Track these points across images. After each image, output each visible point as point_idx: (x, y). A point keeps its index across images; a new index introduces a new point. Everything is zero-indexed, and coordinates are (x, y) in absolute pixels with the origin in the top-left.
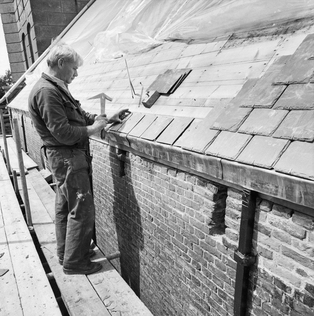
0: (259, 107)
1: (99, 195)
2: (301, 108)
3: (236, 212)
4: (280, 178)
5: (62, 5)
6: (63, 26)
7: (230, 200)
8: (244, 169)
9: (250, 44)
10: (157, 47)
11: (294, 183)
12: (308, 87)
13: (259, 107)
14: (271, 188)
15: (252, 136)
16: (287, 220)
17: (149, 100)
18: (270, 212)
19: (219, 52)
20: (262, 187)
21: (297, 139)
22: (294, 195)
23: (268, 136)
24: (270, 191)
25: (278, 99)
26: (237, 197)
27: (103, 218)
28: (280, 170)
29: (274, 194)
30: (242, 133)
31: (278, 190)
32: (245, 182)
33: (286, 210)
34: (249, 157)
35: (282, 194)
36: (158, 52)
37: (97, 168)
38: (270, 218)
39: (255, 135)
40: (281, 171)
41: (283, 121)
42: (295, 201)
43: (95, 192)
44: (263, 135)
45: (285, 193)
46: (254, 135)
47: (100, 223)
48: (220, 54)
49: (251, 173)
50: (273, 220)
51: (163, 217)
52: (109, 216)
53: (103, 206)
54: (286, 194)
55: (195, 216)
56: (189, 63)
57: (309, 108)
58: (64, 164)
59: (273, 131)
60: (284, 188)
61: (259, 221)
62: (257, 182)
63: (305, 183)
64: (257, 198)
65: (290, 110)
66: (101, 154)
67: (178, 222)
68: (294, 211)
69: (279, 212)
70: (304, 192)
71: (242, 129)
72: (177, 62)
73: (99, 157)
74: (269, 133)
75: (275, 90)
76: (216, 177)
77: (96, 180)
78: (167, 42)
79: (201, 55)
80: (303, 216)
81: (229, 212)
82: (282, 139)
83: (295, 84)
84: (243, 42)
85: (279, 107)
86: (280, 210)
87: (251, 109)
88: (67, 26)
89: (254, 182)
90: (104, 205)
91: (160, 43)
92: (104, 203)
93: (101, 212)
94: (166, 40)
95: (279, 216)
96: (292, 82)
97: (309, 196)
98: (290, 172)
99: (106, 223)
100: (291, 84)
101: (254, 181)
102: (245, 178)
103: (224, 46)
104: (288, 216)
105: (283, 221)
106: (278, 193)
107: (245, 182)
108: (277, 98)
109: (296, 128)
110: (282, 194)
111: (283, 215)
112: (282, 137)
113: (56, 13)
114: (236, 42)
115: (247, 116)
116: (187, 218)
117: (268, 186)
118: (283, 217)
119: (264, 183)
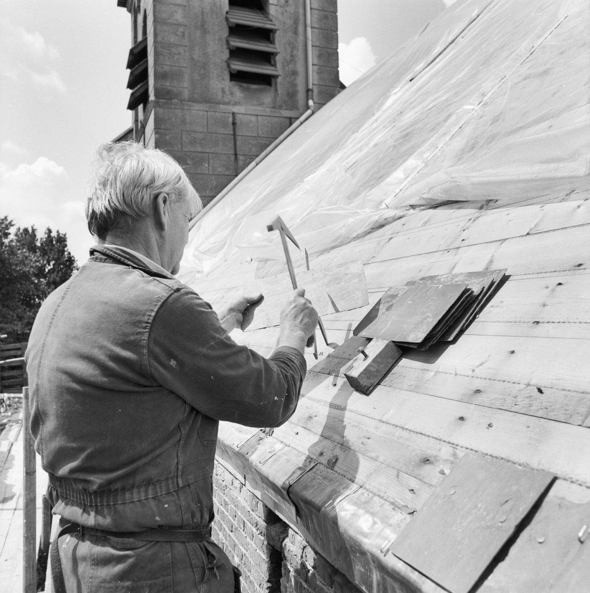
5: (211, 161)
6: (209, 197)
10: (389, 223)
17: (366, 370)
36: (393, 236)
72: (450, 258)
78: (417, 209)
79: (528, 237)
88: (215, 197)
91: (399, 213)
94: (413, 207)
113: (200, 174)
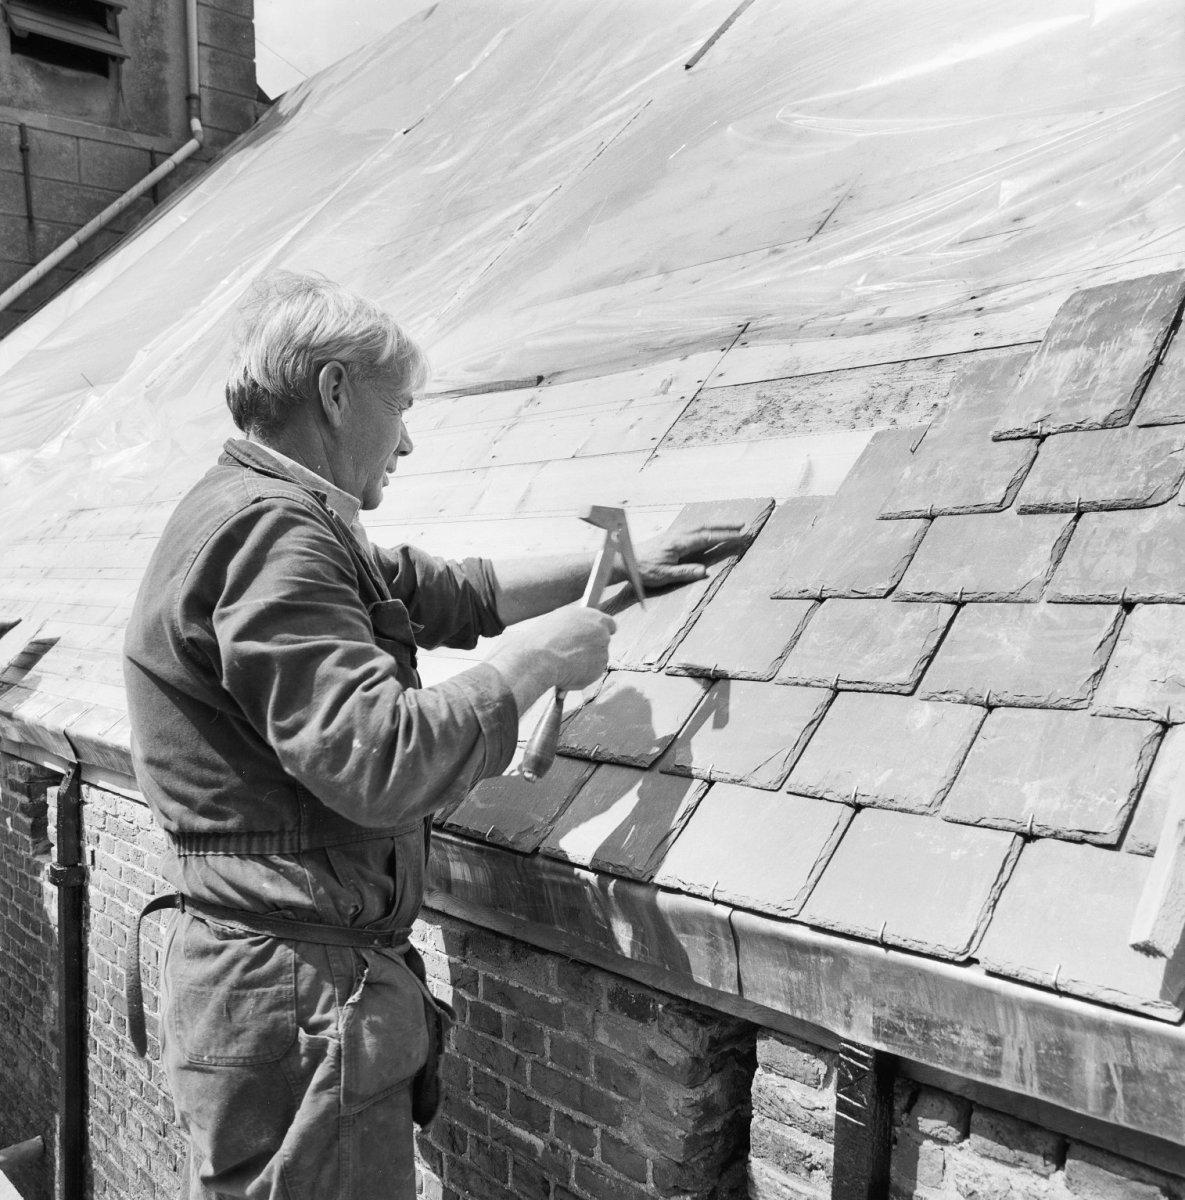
0: (858, 688)
1: (117, 1040)
2: (1036, 700)
3: (801, 1142)
4: (1009, 1003)
7: (771, 1088)
8: (839, 958)
9: (770, 435)
11: (1072, 1027)
12: (1043, 616)
13: (858, 688)
14: (970, 1042)
15: (851, 811)
16: (1043, 1180)
18: (961, 1145)
19: (648, 454)
20: (927, 1039)
21: (1049, 832)
22: (1075, 1077)
23: (922, 814)
24: (963, 1059)
25: (931, 658)
26: (801, 1073)
27: (133, 1147)
28: (1007, 970)
29: (987, 1073)
30: (806, 796)
31: (1001, 1053)
32: (847, 1013)
33: (1034, 1135)
34: (851, 904)
35: (1021, 1070)
37: (117, 915)
38: (961, 1170)
39: (864, 807)
40: (1014, 973)
41: (969, 749)
42: (1085, 1106)
43: (95, 1023)
44: (902, 811)
45: (1034, 1066)
46: (858, 808)
47: (111, 1174)
48: (656, 463)
49: (875, 976)
50: (976, 1180)
51: (440, 1155)
52: (160, 1138)
53: (133, 1093)
54: (1039, 1071)
55: (597, 1149)
56: (529, 491)
57: (1069, 702)
58: (296, 1042)
59: (942, 794)
60: (1030, 1045)
61: (915, 1188)
62: (901, 1017)
63: (1127, 1032)
64: (898, 1082)
65: (990, 708)
66: (138, 855)
67: (514, 1176)
68: (1068, 1141)
69: (1003, 1149)
70: (1123, 1067)
71: (806, 776)
73: (130, 865)
74: (928, 802)
75: (914, 622)
76: (710, 985)
77: (102, 967)
80: (1115, 1168)
81: (770, 1139)
82: (985, 827)
83: (989, 601)
84: (745, 427)
85: (944, 693)
86: (1007, 1138)
87: (827, 694)
89: (885, 1013)
90: (141, 1088)
92: (142, 1078)
93: (124, 1122)
95: (1004, 1162)
96: (976, 595)
97: (1148, 1087)
98: (1053, 979)
99: (144, 1175)
100: (971, 602)
101: (887, 1010)
102: (848, 998)
103: (669, 435)
104: (1045, 1165)
105: (1023, 1188)
106: (1003, 1069)
107: (847, 1013)
108: (927, 652)
109: (1037, 784)
110: (1021, 1070)
111: (1021, 1160)
112: (983, 823)
114: (714, 424)
115: (816, 722)
116: (561, 1161)
117: (953, 1036)
118: (1022, 1169)
119: (935, 1019)
